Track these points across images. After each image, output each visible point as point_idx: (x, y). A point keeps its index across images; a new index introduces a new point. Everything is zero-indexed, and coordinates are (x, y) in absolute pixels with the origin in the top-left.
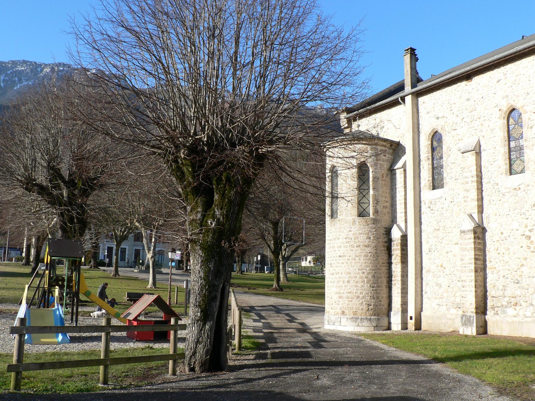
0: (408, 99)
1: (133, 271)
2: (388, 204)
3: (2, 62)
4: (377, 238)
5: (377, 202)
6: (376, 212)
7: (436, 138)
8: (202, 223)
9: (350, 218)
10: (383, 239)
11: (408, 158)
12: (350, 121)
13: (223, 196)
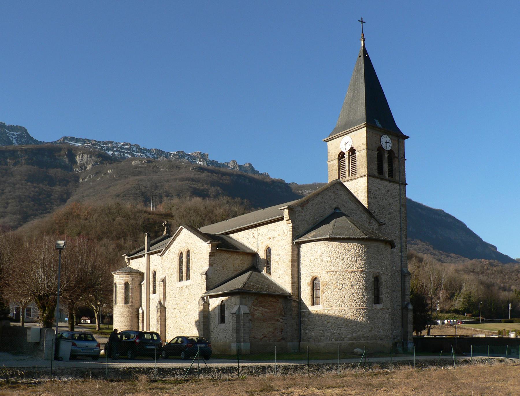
0: (146, 255)
1: (36, 325)
2: (138, 299)
3: (1, 125)
4: (132, 313)
5: (132, 298)
6: (132, 302)
7: (155, 273)
8: (43, 315)
9: (121, 305)
10: (135, 313)
11: (145, 282)
12: (129, 260)
13: (48, 308)
